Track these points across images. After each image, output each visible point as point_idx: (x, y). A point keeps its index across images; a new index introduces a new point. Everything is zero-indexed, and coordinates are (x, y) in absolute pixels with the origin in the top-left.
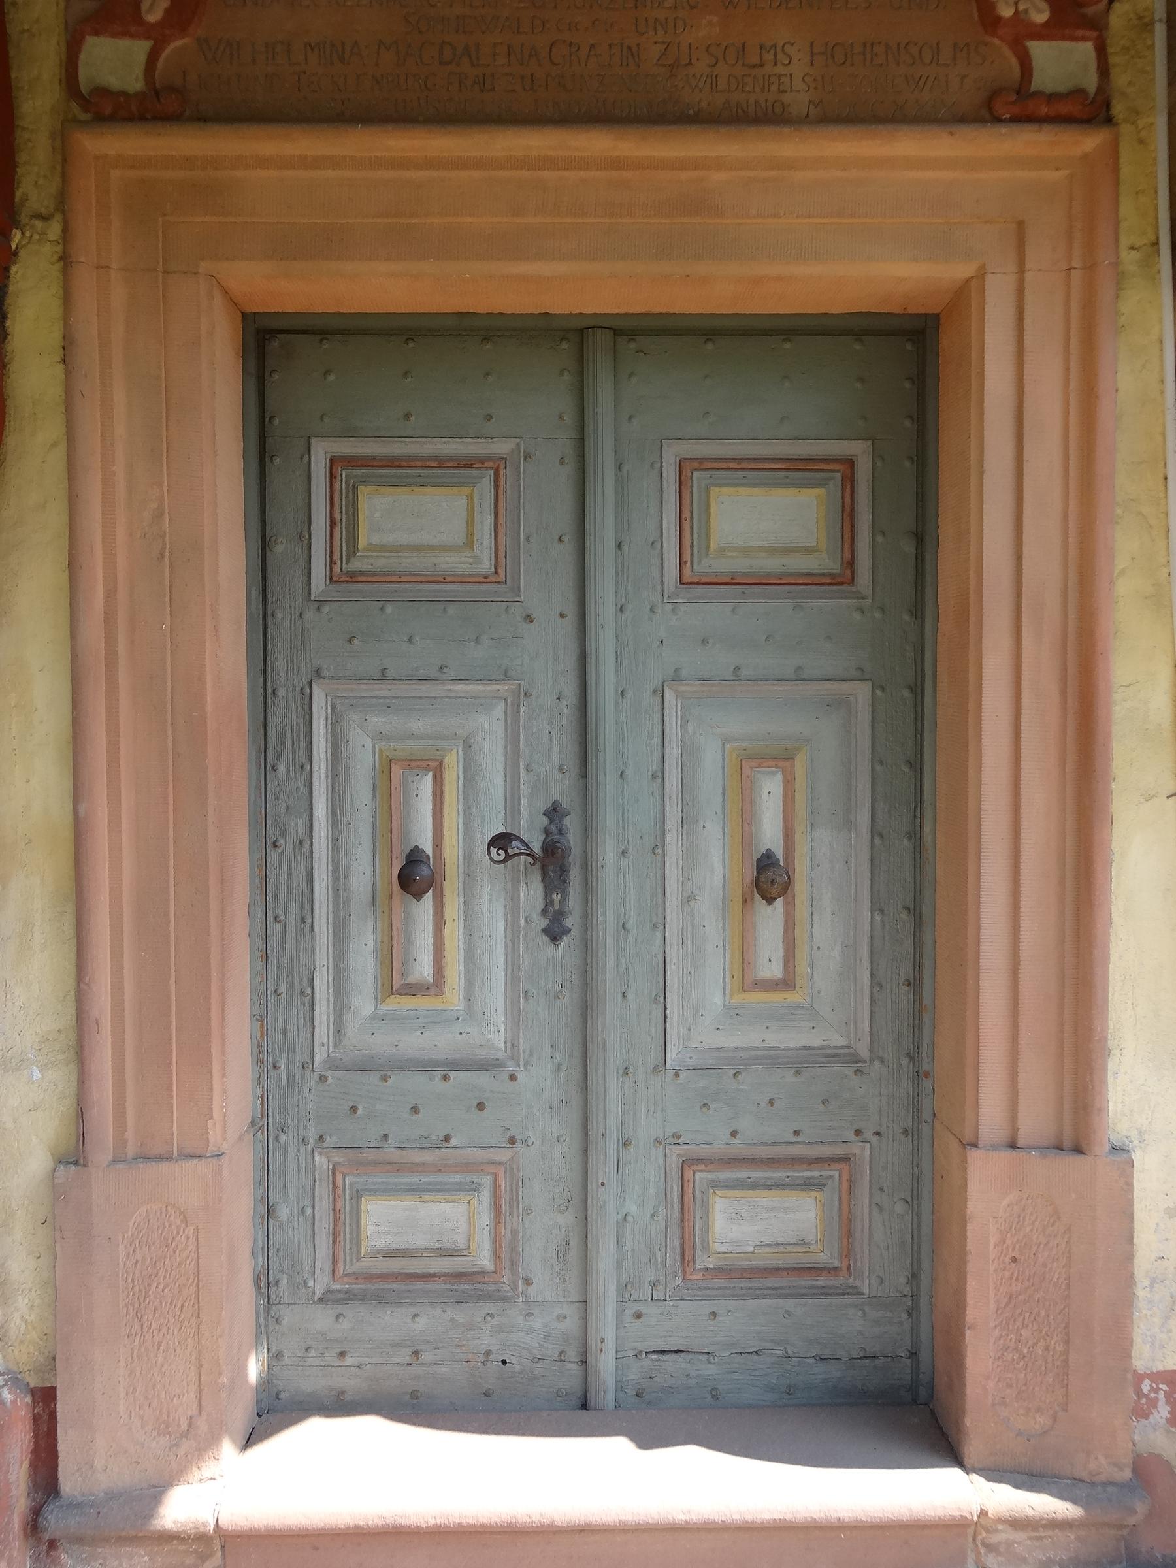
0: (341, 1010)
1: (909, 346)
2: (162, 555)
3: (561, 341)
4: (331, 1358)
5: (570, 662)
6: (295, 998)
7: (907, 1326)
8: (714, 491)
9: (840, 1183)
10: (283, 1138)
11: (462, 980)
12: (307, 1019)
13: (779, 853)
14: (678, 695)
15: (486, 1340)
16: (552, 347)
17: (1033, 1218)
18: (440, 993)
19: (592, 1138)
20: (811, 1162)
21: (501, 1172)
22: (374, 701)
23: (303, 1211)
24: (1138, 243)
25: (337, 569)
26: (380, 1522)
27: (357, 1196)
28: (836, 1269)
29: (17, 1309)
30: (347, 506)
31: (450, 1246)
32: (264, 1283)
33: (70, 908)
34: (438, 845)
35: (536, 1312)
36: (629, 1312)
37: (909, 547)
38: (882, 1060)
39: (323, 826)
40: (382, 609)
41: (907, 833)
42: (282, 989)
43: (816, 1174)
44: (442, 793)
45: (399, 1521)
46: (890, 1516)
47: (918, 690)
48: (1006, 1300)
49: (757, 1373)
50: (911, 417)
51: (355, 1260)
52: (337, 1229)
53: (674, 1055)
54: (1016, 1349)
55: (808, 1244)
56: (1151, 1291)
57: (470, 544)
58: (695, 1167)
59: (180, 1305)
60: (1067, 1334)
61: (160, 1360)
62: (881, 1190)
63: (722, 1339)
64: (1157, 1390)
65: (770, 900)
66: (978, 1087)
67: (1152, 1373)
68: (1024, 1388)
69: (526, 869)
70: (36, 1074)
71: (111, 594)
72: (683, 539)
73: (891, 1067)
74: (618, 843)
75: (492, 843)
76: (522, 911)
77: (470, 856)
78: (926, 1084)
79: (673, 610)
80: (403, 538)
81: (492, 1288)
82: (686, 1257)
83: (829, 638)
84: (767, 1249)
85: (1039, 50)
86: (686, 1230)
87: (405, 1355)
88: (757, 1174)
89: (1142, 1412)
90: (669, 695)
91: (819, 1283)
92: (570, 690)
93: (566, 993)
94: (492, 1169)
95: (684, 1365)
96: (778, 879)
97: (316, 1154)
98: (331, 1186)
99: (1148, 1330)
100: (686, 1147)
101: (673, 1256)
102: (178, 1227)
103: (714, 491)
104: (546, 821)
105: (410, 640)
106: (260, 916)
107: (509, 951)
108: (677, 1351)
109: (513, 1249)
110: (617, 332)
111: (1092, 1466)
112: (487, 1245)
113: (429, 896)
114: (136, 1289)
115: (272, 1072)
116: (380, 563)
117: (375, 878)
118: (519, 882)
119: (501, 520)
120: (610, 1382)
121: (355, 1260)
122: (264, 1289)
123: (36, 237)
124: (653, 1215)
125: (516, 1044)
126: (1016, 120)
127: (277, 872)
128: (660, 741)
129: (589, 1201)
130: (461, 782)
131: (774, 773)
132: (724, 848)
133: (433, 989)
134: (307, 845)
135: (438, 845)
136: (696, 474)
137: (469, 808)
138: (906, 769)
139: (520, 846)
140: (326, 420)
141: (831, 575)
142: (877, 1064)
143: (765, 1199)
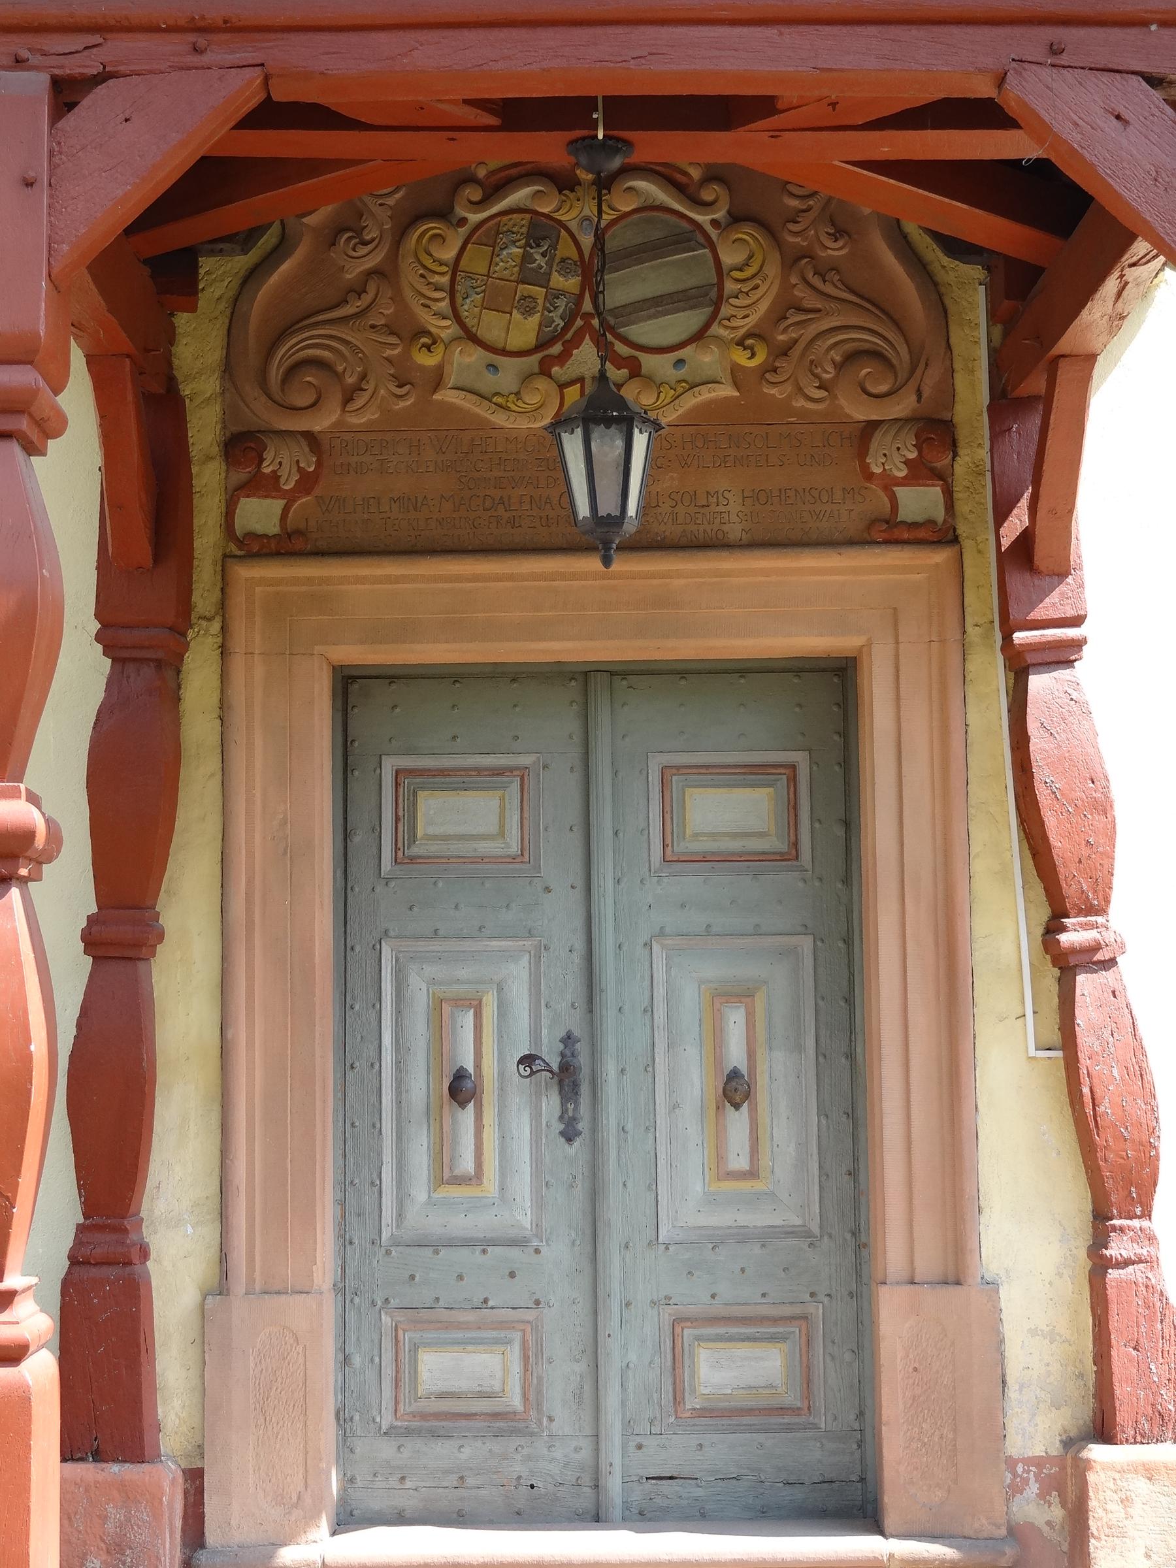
0: (402, 1198)
1: (836, 680)
2: (285, 853)
3: (570, 680)
4: (394, 1482)
5: (579, 922)
6: (367, 1187)
7: (857, 1455)
8: (688, 791)
9: (800, 1337)
10: (357, 1300)
11: (497, 1172)
12: (376, 1204)
13: (744, 1070)
14: (663, 947)
15: (518, 1468)
16: (563, 685)
17: (928, 1336)
18: (480, 1183)
19: (600, 1299)
20: (775, 1320)
21: (529, 1330)
22: (428, 955)
23: (372, 1360)
24: (980, 622)
25: (400, 853)
26: (443, 1561)
27: (415, 1348)
28: (799, 1409)
29: (173, 1408)
30: (408, 807)
31: (488, 1390)
32: (342, 1418)
33: (217, 1107)
34: (478, 1065)
35: (557, 1444)
36: (632, 1444)
37: (840, 831)
38: (830, 1236)
39: (389, 1052)
40: (435, 883)
41: (846, 1054)
42: (356, 1181)
43: (781, 1330)
44: (481, 1025)
45: (457, 1560)
46: (821, 1557)
47: (848, 941)
48: (911, 1401)
49: (737, 1495)
50: (839, 733)
51: (413, 1401)
52: (399, 1375)
53: (665, 1233)
54: (919, 1439)
55: (776, 1387)
56: (1021, 1393)
57: (501, 833)
58: (683, 1324)
59: (292, 1405)
60: (955, 1424)
61: (278, 1446)
62: (833, 1342)
63: (709, 1466)
64: (1028, 1472)
65: (737, 1106)
66: (885, 1238)
67: (1024, 1458)
68: (926, 1469)
69: (546, 1084)
70: (190, 1230)
71: (250, 881)
72: (666, 828)
73: (838, 1242)
74: (618, 1063)
75: (520, 1062)
76: (544, 1117)
77: (503, 1074)
78: (864, 1252)
79: (658, 882)
80: (451, 830)
81: (523, 1425)
82: (678, 1398)
83: (780, 902)
84: (741, 1391)
85: (901, 492)
86: (677, 1376)
87: (452, 1480)
88: (734, 1330)
89: (1016, 1489)
90: (656, 947)
91: (786, 1421)
92: (579, 944)
93: (579, 1183)
94: (522, 1326)
95: (678, 1488)
96: (740, 1087)
97: (382, 1313)
98: (394, 1341)
99: (1020, 1424)
100: (676, 1306)
101: (667, 1397)
102: (292, 1346)
103: (688, 791)
104: (561, 1046)
105: (456, 907)
106: (341, 1123)
107: (534, 1149)
108: (671, 1478)
109: (539, 1392)
110: (612, 674)
111: (976, 1525)
112: (518, 1390)
113: (472, 1104)
114: (261, 1391)
115: (348, 1247)
116: (434, 848)
117: (429, 1093)
118: (541, 1095)
119: (526, 815)
120: (618, 1501)
121: (413, 1401)
122: (342, 1422)
123: (202, 632)
124: (650, 1363)
125: (540, 1224)
126: (888, 542)
127: (353, 1088)
128: (649, 983)
129: (599, 1351)
130: (495, 1017)
131: (739, 1007)
132: (701, 1066)
133: (474, 1181)
134: (377, 1066)
135: (478, 1065)
136: (674, 778)
137: (502, 1037)
138: (842, 1004)
139: (542, 1063)
140: (393, 741)
141: (781, 854)
142: (826, 1238)
143: (742, 1351)
